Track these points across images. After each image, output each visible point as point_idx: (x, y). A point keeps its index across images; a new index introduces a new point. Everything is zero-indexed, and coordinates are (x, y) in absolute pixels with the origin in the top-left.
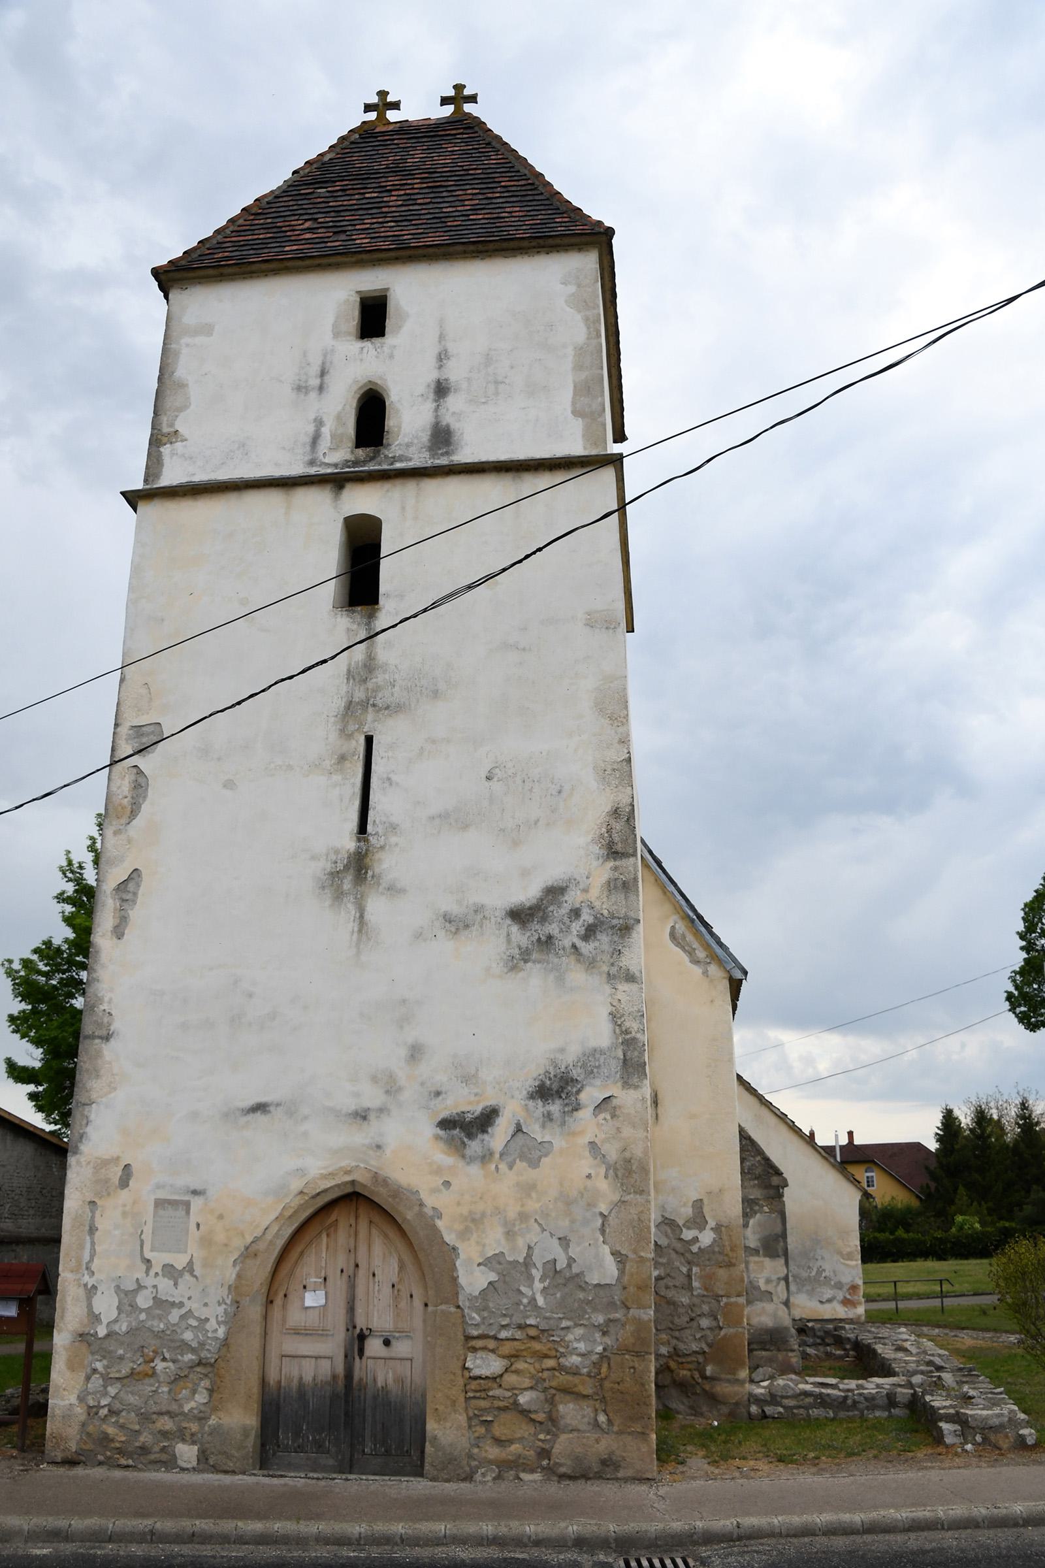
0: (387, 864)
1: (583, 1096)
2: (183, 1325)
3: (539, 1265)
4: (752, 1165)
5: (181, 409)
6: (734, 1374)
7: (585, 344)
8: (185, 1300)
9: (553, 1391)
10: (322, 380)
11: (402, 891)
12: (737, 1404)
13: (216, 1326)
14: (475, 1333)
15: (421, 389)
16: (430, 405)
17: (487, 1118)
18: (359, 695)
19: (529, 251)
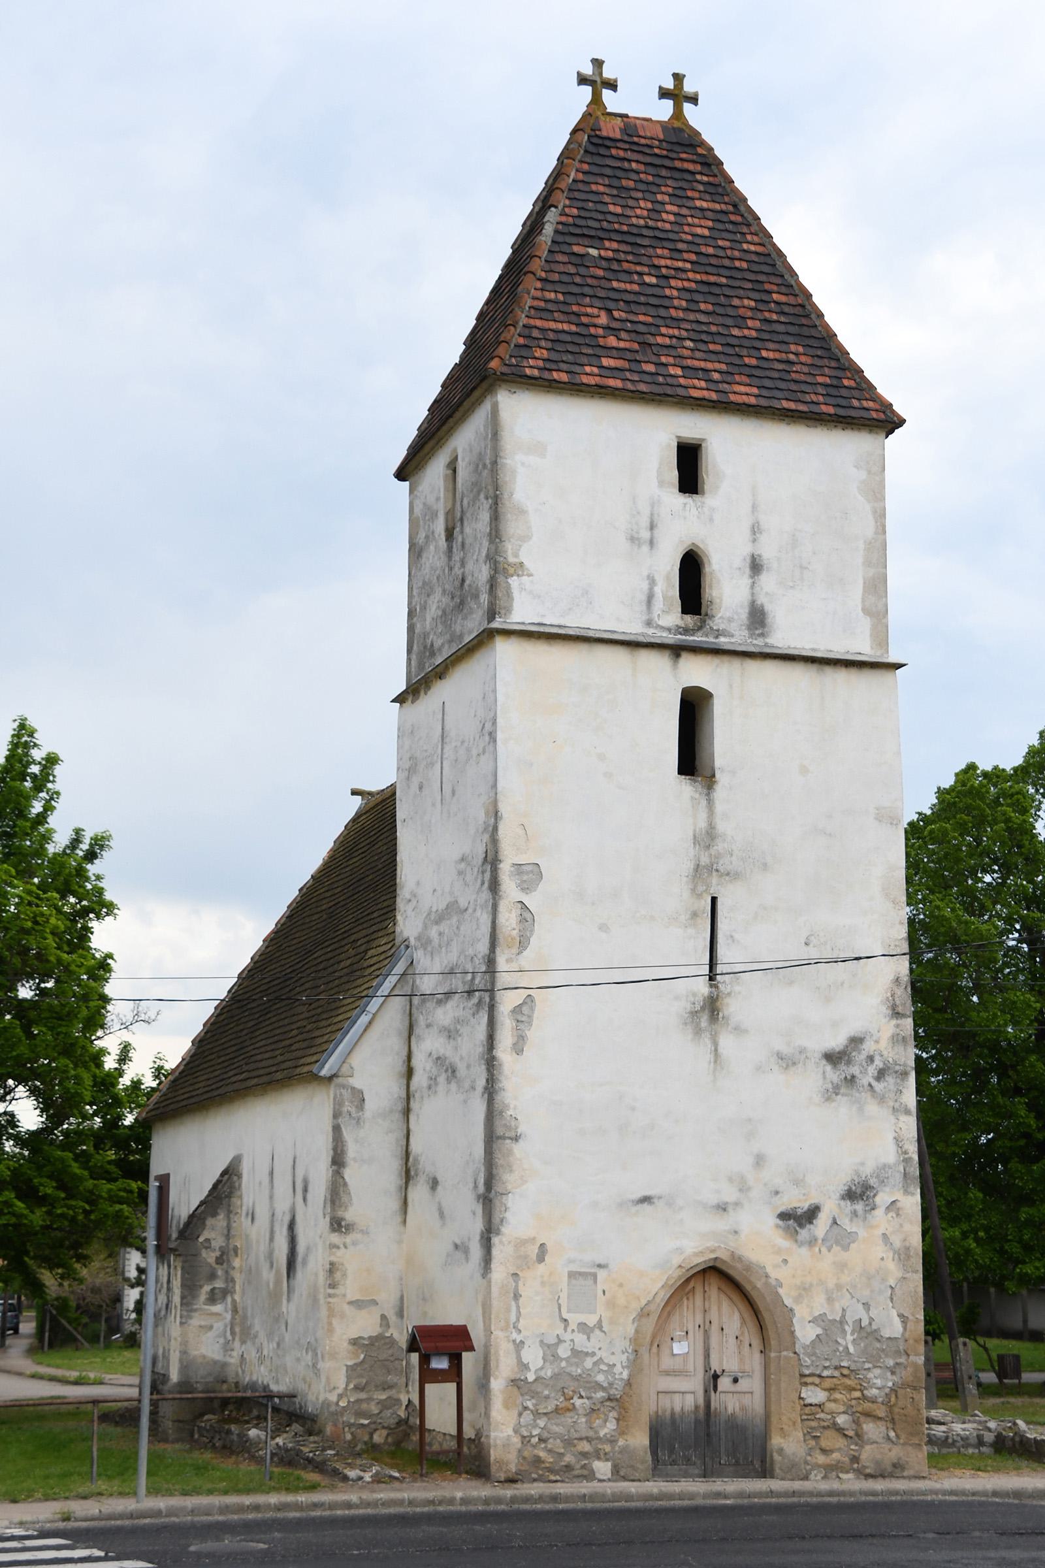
0: (732, 1008)
1: (878, 1199)
2: (596, 1368)
3: (850, 1323)
5: (526, 538)
8: (596, 1350)
9: (858, 1415)
11: (746, 1031)
13: (621, 1370)
14: (807, 1372)
16: (746, 581)
17: (812, 1214)
18: (705, 860)
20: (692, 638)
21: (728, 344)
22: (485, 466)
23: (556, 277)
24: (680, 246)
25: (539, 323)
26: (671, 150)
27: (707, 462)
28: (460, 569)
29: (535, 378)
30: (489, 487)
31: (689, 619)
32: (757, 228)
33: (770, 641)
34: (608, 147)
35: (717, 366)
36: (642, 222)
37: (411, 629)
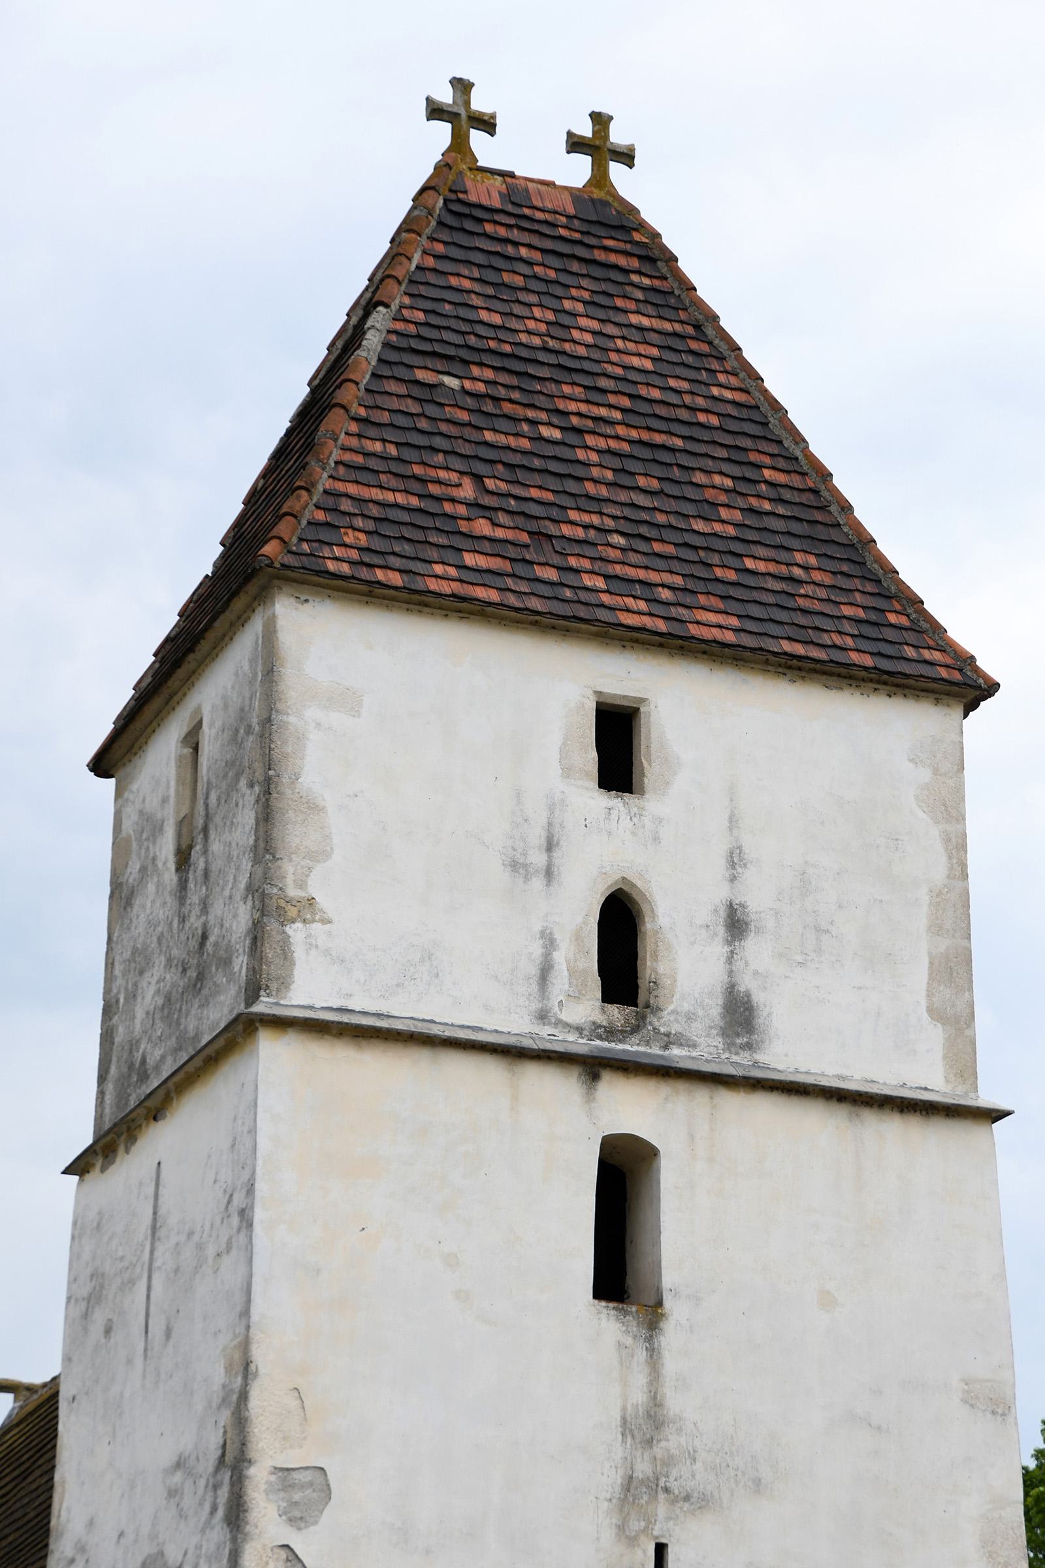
5: (321, 855)
7: (945, 886)
10: (549, 857)
15: (704, 915)
16: (718, 949)
18: (643, 1468)
19: (863, 684)
20: (620, 1046)
21: (686, 545)
22: (249, 730)
23: (385, 417)
24: (603, 383)
25: (352, 489)
26: (588, 233)
27: (648, 738)
28: (199, 917)
29: (343, 578)
30: (256, 765)
31: (617, 1014)
32: (736, 364)
33: (761, 1057)
34: (480, 221)
35: (667, 578)
36: (536, 341)
37: (107, 1037)
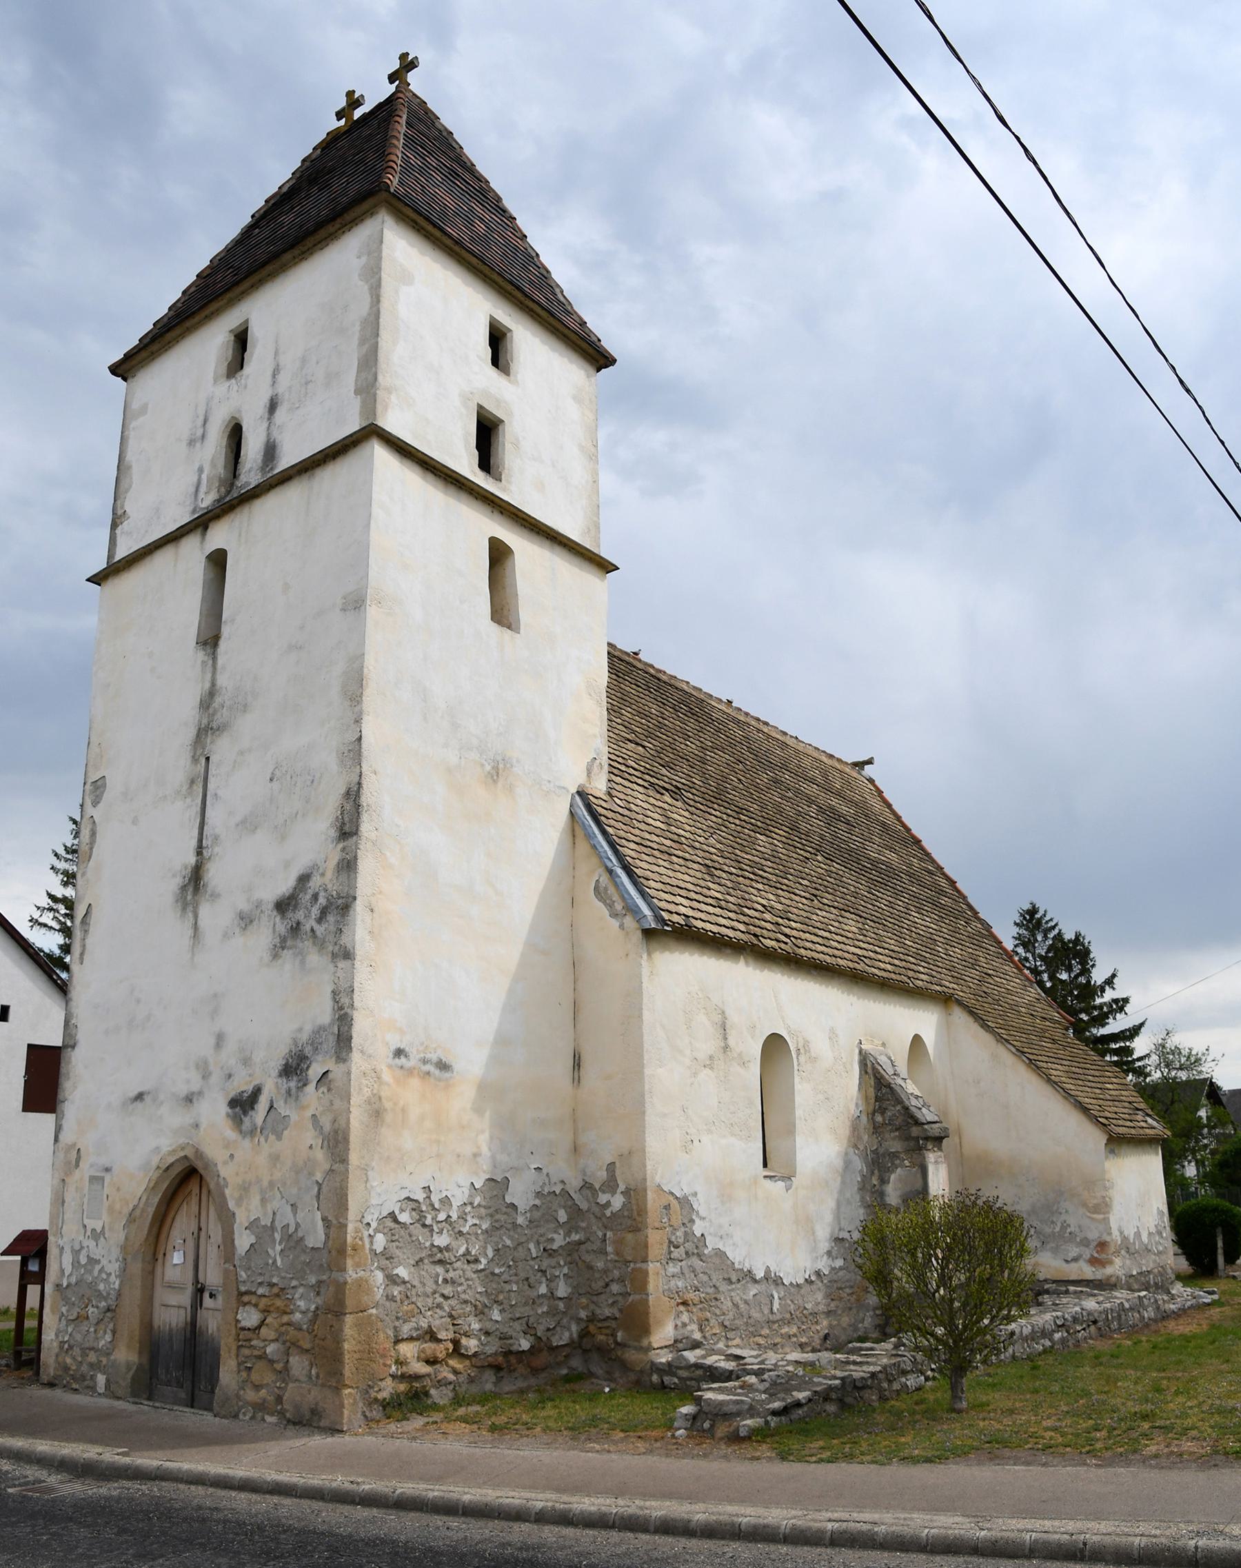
1: (310, 1072)
3: (279, 1230)
4: (893, 1115)
6: (639, 1342)
12: (642, 1372)
